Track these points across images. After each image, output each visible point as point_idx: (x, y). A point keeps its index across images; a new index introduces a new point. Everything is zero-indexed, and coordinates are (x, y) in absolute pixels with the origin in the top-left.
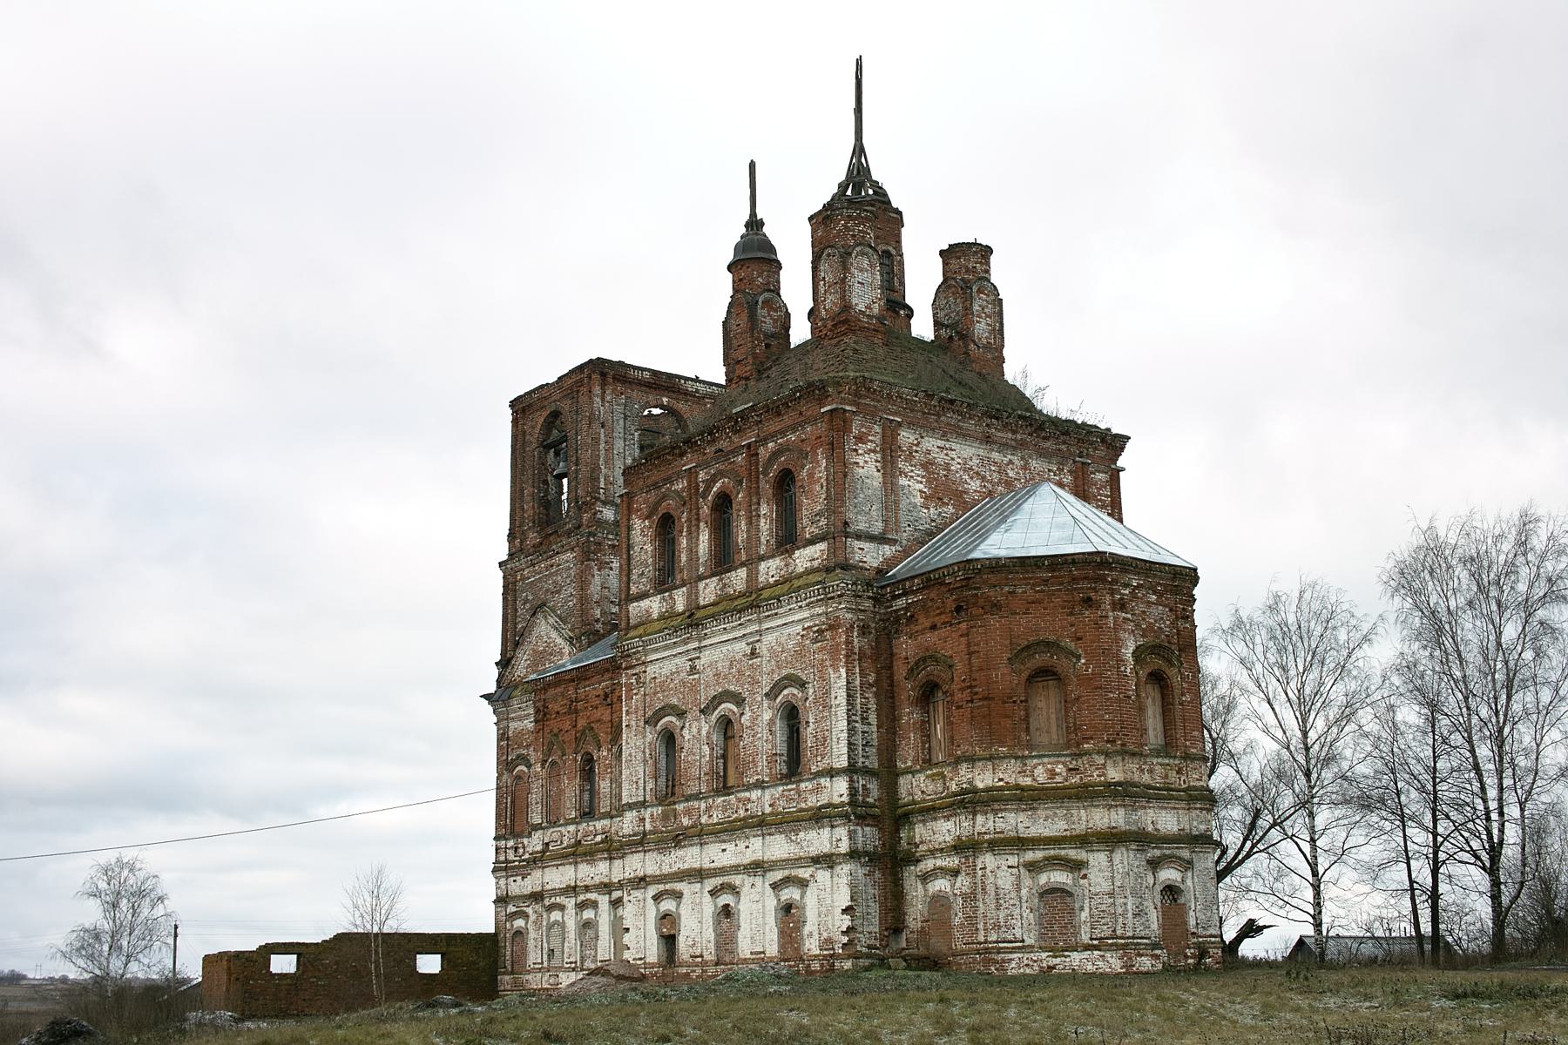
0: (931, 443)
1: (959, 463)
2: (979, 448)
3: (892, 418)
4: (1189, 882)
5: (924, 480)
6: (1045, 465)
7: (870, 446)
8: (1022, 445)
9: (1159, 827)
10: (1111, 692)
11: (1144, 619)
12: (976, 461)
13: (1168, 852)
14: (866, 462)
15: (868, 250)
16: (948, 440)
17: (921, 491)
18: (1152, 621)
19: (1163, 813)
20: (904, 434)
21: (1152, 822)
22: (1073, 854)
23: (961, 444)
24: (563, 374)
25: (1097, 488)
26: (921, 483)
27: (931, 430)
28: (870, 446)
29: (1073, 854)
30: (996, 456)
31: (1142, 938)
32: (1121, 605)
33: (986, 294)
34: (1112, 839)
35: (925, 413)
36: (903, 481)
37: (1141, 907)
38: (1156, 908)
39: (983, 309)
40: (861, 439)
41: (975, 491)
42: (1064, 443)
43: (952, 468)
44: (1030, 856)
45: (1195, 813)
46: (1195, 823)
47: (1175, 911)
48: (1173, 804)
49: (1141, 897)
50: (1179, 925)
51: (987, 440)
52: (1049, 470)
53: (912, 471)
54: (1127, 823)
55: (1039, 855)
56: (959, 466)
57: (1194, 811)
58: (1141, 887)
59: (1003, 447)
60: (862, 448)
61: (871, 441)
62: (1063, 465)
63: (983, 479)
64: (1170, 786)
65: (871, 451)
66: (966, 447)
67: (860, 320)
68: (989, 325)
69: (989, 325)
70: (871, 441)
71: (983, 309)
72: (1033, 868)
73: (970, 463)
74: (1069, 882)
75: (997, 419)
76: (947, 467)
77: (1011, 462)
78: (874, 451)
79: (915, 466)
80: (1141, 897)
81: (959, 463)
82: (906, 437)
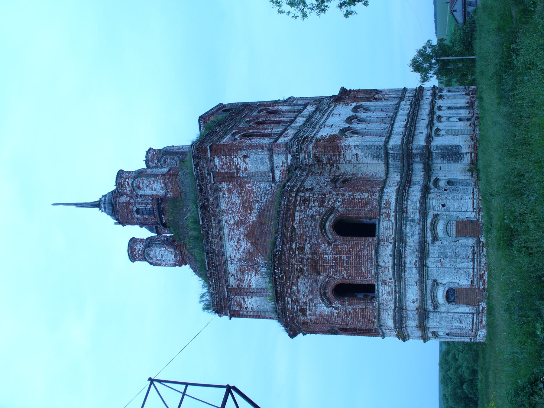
0: (231, 268)
1: (236, 253)
2: (225, 241)
3: (226, 293)
4: (444, 282)
5: (249, 273)
6: (222, 200)
7: (242, 301)
8: (215, 215)
9: (415, 299)
10: (348, 321)
11: (307, 296)
12: (232, 243)
13: (429, 295)
14: (250, 304)
15: (146, 253)
16: (227, 259)
17: (255, 275)
18: (307, 291)
19: (408, 295)
20: (231, 282)
21: (413, 302)
22: (429, 220)
23: (226, 252)
24: (204, 113)
25: (224, 165)
26: (251, 275)
27: (225, 269)
28: (242, 301)
29: (429, 220)
30: (226, 231)
31: (473, 320)
32: (303, 311)
33: (140, 184)
34: (422, 267)
35: (218, 273)
36: (253, 285)
37: (458, 319)
38: (458, 308)
39: (148, 186)
40: (240, 305)
41: (247, 245)
42: (206, 188)
43: (239, 257)
44: (429, 239)
45: (407, 276)
46: (413, 276)
47: (460, 294)
48: (403, 291)
49: (452, 318)
50: (467, 292)
51: (220, 237)
52: (223, 197)
53: (247, 279)
54: (414, 320)
55: (429, 234)
56: (237, 253)
57: (406, 276)
58: (447, 318)
59: (221, 228)
60: (244, 305)
61: (240, 300)
62: (218, 188)
63: (239, 239)
64: (393, 290)
65: (244, 301)
66: (227, 249)
67: (179, 260)
68: (154, 183)
69: (154, 183)
70: (240, 300)
71: (148, 186)
72: (436, 307)
73: (234, 246)
74: (443, 289)
75: (208, 233)
76: (240, 260)
77: (226, 222)
78: (244, 299)
79: (244, 278)
80: (452, 318)
81: (236, 253)
82: (232, 282)
